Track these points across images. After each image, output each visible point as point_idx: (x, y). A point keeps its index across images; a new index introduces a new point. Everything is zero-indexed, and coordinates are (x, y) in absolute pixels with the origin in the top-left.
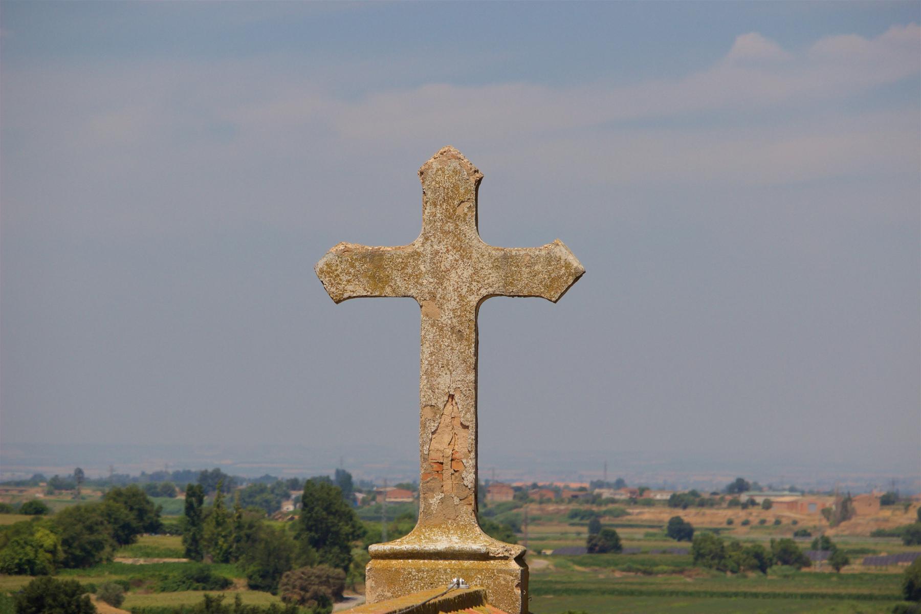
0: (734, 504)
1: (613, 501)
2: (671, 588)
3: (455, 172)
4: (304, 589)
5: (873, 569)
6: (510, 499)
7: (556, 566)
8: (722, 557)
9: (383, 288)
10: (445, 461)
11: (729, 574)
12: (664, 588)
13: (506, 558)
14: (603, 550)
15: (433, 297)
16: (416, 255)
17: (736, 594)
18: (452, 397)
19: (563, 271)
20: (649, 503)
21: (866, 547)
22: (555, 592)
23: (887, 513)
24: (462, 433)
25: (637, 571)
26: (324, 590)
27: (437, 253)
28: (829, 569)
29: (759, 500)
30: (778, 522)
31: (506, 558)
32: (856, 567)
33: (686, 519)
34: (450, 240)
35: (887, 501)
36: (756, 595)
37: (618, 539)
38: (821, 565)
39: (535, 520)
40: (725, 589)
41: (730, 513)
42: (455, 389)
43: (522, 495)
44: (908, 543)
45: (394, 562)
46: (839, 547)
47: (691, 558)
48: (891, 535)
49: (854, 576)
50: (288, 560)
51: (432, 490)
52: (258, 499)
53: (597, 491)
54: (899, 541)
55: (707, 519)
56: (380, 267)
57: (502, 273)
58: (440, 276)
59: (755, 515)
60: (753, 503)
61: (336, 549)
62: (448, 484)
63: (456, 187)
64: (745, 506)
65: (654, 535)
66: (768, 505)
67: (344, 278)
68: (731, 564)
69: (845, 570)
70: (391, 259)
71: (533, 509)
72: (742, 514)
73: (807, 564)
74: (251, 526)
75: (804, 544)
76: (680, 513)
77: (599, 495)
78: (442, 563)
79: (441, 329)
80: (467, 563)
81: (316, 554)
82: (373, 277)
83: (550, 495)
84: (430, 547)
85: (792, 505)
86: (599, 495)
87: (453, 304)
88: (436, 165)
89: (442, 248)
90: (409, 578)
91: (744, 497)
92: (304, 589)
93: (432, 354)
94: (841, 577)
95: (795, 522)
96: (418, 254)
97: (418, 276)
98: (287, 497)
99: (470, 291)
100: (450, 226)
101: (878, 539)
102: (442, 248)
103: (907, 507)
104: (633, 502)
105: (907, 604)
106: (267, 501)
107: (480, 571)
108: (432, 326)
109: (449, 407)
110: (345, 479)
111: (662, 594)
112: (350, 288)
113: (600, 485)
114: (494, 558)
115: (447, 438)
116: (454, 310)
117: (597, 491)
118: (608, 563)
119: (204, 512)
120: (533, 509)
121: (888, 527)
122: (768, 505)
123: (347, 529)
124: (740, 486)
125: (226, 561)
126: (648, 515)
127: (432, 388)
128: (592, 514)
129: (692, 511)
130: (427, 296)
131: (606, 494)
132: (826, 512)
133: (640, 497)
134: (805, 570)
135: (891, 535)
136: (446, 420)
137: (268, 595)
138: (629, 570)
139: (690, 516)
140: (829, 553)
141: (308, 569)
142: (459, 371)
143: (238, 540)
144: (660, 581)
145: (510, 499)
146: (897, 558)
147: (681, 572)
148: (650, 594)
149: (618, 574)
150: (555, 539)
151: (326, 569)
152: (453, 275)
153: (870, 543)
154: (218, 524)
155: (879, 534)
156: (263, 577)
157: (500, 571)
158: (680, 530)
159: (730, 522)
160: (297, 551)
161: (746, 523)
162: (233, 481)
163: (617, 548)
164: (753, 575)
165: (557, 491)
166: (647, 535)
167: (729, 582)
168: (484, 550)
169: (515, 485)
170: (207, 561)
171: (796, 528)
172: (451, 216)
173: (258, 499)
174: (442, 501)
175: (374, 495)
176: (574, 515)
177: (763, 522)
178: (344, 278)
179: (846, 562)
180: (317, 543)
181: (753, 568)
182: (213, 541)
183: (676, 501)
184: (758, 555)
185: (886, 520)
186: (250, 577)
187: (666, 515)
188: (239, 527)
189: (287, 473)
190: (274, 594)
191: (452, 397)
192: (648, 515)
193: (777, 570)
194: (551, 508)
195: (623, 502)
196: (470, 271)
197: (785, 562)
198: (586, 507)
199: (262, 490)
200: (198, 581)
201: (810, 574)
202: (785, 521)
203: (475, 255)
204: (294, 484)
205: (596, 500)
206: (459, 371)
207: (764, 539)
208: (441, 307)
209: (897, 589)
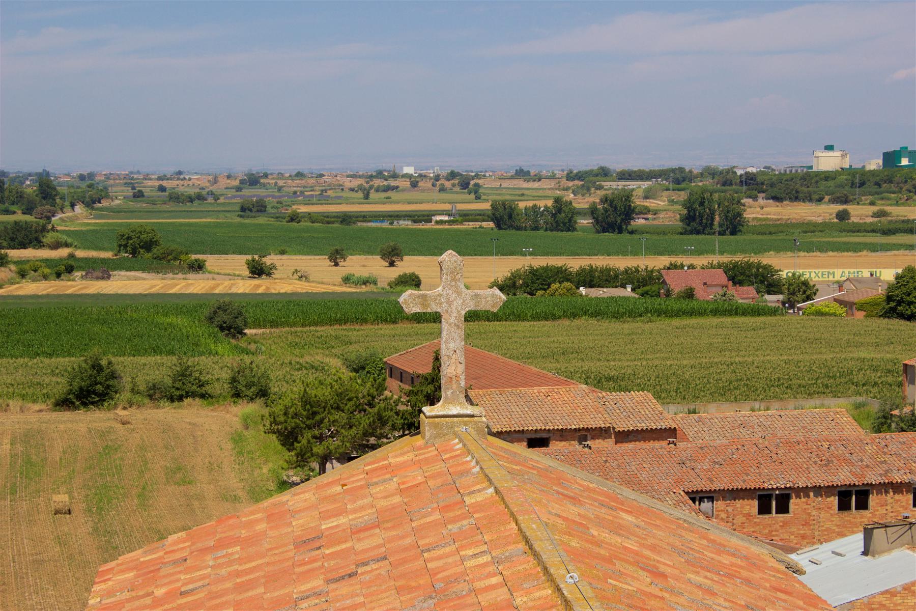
0: (179, 179)
1: (138, 179)
2: (163, 210)
3: (455, 261)
4: (42, 214)
5: (227, 201)
6: (103, 179)
7: (123, 202)
8: (178, 199)
9: (427, 309)
10: (453, 377)
11: (181, 204)
12: (160, 210)
13: (481, 416)
14: (138, 197)
15: (447, 312)
16: (440, 295)
17: (185, 211)
18: (455, 351)
19: (498, 300)
20: (150, 179)
21: (224, 193)
22: (125, 212)
23: (229, 181)
24: (460, 366)
25: (150, 203)
26: (49, 214)
27: (448, 294)
28: (213, 201)
29: (187, 177)
30: (194, 185)
31: (481, 416)
32: (222, 200)
33: (164, 185)
34: (453, 288)
35: (229, 177)
36: (191, 211)
37: (143, 193)
38: (210, 200)
39: (112, 186)
40: (180, 210)
41: (177, 182)
42: (457, 348)
43: (108, 177)
44: (237, 191)
45: (436, 419)
46: (216, 193)
47: (168, 199)
48: (231, 188)
49: (221, 203)
50: (35, 204)
51: (448, 389)
52: (17, 180)
53: (132, 175)
54: (234, 190)
55: (170, 184)
56: (426, 300)
57: (474, 301)
58: (450, 303)
59: (186, 183)
60: (185, 179)
61: (51, 200)
62: (454, 386)
63: (455, 268)
64: (182, 180)
65: (153, 190)
66: (190, 179)
67: (412, 305)
68: (181, 200)
69: (218, 201)
70: (430, 297)
71: (112, 182)
72: (181, 183)
73: (206, 200)
74: (21, 192)
75: (204, 193)
76: (161, 182)
77: (133, 177)
78: (456, 419)
79: (451, 325)
80: (465, 419)
81: (44, 202)
82: (423, 304)
83: (117, 177)
84: (451, 413)
85: (198, 179)
86: (133, 177)
87: (455, 315)
88: (447, 259)
89: (450, 292)
90: (443, 425)
91: (182, 177)
92: (42, 214)
93: (447, 334)
94: (218, 204)
95: (199, 185)
96: (441, 295)
97: (441, 304)
98: (27, 179)
99: (462, 309)
100: (453, 283)
101: (226, 190)
102: (450, 292)
103: (236, 179)
104: (145, 179)
105: (241, 213)
106: (21, 181)
107: (471, 422)
108: (447, 323)
109: (454, 356)
110: (48, 174)
111: (160, 212)
112: (414, 309)
113: (132, 173)
114: (476, 417)
115: (453, 368)
116: (456, 317)
117: (132, 175)
118: (141, 201)
119: (5, 188)
120: (112, 182)
121: (229, 186)
122: (190, 179)
123: (54, 193)
124: (180, 173)
125: (13, 204)
126: (150, 183)
127: (447, 348)
128: (132, 183)
129: (165, 182)
130: (445, 312)
131: (136, 176)
132: (209, 181)
133: (147, 177)
134: (205, 202)
135: (231, 188)
136: (453, 360)
137: (29, 216)
138: (148, 203)
139: (165, 184)
140: (213, 196)
141: (43, 207)
142: (458, 341)
143: (17, 197)
144: (159, 207)
145: (103, 179)
146: (234, 197)
147: (165, 204)
148: (155, 212)
149: (144, 205)
150: (120, 192)
151: (48, 207)
152: (455, 302)
153: (225, 192)
154: (10, 192)
155: (227, 188)
156: (27, 210)
157: (479, 422)
158: (162, 189)
159: (178, 185)
160: (38, 201)
161: (183, 185)
162: (9, 173)
163: (143, 196)
164: (189, 204)
165: (118, 175)
166: (151, 190)
167: (181, 207)
168: (472, 413)
169: (104, 173)
170: (7, 204)
171: (200, 187)
172: (453, 279)
173: (17, 180)
174: (452, 393)
175: (57, 178)
176: (126, 184)
177: (189, 185)
178: (412, 305)
179: (219, 199)
180: (44, 198)
181: (188, 202)
182: (8, 198)
183: (159, 179)
184: (190, 198)
185: (229, 184)
186: (22, 210)
187: (157, 183)
188: (17, 193)
189: (27, 169)
190: (31, 215)
191: (455, 351)
192: (150, 183)
193: (196, 202)
194: (118, 181)
195: (142, 179)
196: (462, 301)
197: (199, 199)
198: (129, 181)
199: (19, 177)
200: (5, 211)
201: (207, 203)
202: (196, 184)
203: (463, 295)
204: (30, 175)
205: (132, 178)
206: (458, 341)
207: (192, 191)
208: (450, 316)
209: (238, 209)
